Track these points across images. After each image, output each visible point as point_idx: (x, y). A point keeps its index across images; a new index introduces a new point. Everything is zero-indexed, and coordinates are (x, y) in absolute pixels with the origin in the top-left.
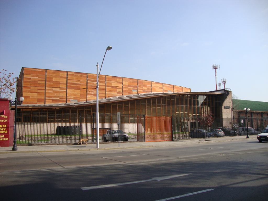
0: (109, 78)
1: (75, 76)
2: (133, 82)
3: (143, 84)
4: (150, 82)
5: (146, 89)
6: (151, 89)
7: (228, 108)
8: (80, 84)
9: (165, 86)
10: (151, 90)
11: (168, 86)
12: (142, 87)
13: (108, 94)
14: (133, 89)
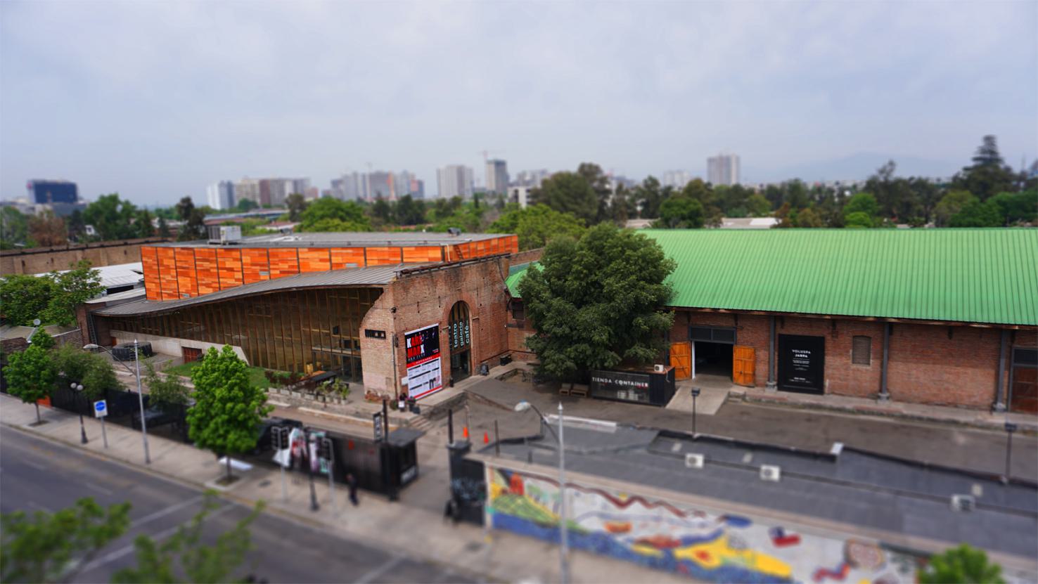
0: (220, 253)
1: (183, 254)
2: (261, 255)
3: (280, 256)
4: (293, 250)
5: (285, 267)
6: (299, 266)
7: (380, 335)
8: (188, 268)
9: (337, 254)
10: (299, 268)
11: (347, 254)
12: (277, 264)
13: (224, 283)
14: (261, 270)
